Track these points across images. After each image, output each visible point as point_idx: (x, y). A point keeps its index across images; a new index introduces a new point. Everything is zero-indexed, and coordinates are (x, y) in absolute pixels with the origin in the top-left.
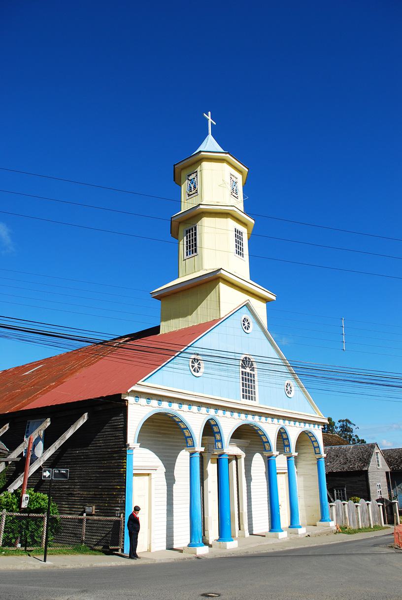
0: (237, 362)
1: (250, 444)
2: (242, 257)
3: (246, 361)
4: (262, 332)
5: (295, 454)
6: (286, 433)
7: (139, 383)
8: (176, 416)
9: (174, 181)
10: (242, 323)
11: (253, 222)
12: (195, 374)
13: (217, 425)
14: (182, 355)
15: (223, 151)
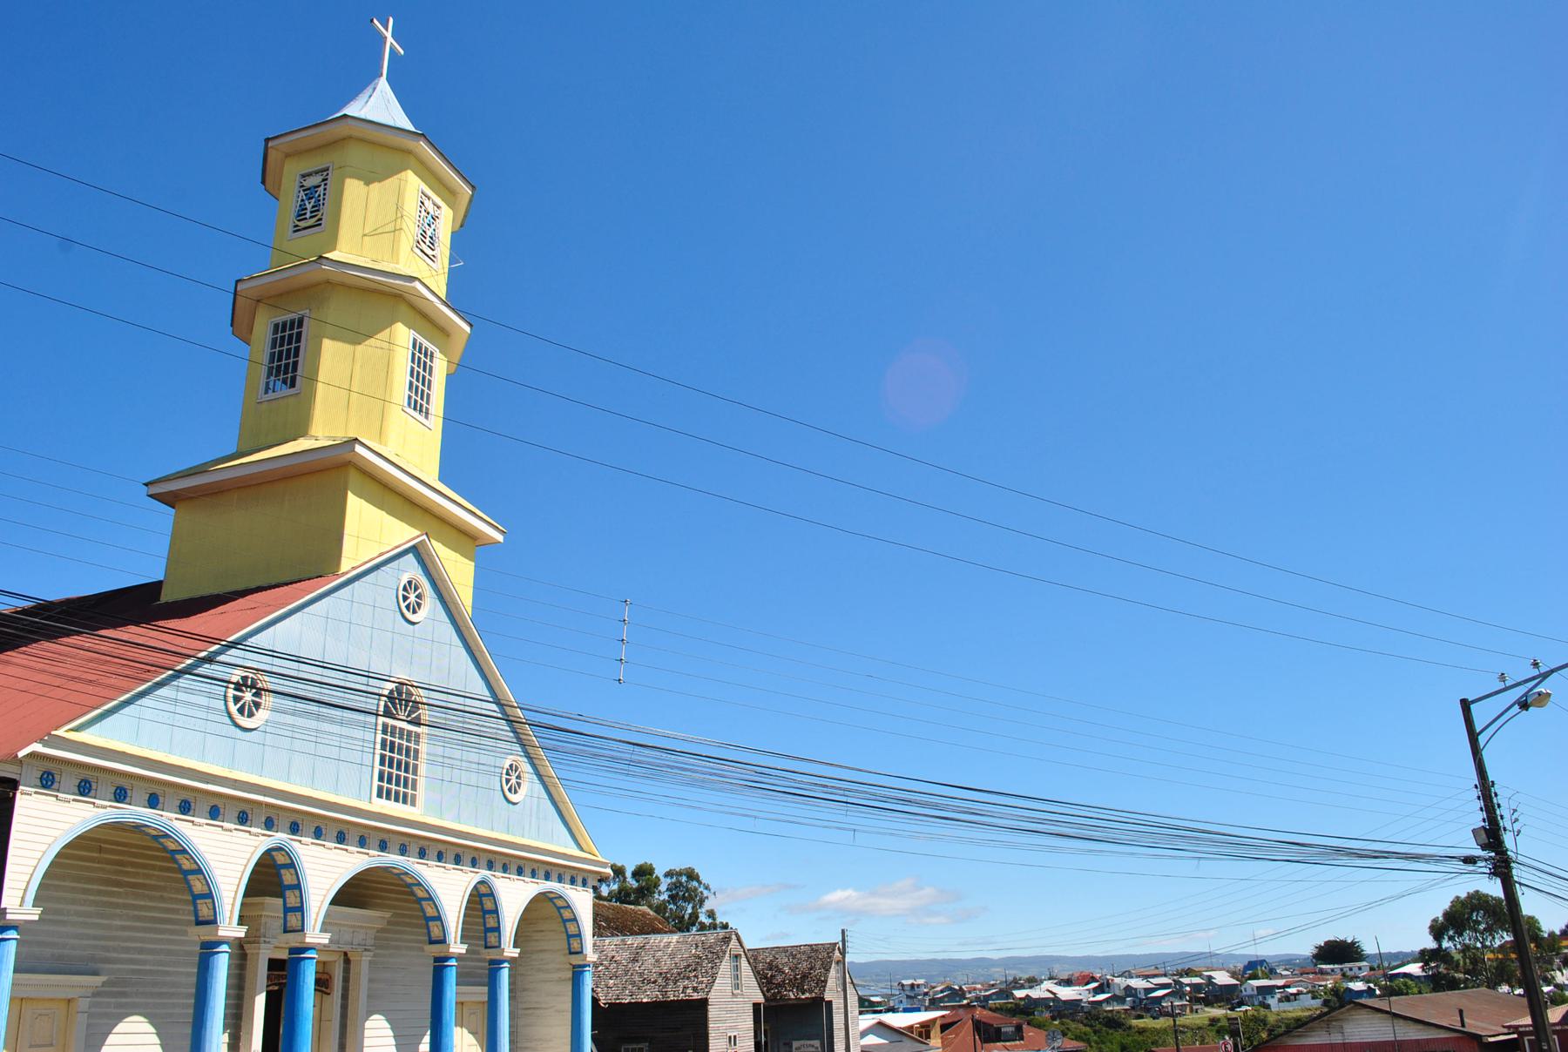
0: (371, 703)
1: (389, 923)
2: (422, 419)
3: (400, 700)
4: (450, 625)
5: (510, 951)
6: (569, 907)
7: (61, 732)
8: (167, 836)
9: (263, 182)
10: (401, 592)
11: (467, 329)
12: (244, 721)
13: (292, 865)
14: (205, 669)
15: (413, 129)
